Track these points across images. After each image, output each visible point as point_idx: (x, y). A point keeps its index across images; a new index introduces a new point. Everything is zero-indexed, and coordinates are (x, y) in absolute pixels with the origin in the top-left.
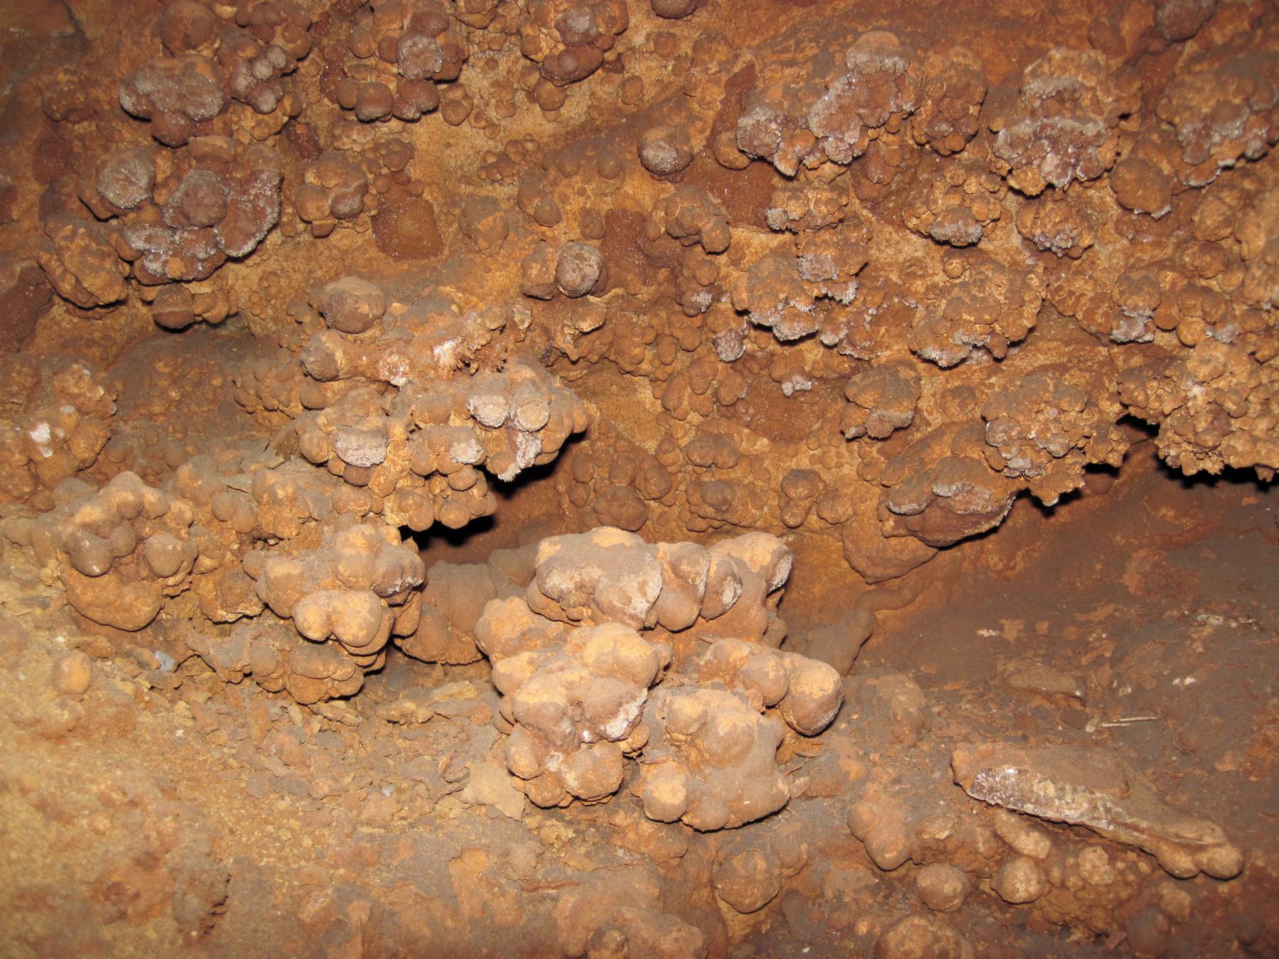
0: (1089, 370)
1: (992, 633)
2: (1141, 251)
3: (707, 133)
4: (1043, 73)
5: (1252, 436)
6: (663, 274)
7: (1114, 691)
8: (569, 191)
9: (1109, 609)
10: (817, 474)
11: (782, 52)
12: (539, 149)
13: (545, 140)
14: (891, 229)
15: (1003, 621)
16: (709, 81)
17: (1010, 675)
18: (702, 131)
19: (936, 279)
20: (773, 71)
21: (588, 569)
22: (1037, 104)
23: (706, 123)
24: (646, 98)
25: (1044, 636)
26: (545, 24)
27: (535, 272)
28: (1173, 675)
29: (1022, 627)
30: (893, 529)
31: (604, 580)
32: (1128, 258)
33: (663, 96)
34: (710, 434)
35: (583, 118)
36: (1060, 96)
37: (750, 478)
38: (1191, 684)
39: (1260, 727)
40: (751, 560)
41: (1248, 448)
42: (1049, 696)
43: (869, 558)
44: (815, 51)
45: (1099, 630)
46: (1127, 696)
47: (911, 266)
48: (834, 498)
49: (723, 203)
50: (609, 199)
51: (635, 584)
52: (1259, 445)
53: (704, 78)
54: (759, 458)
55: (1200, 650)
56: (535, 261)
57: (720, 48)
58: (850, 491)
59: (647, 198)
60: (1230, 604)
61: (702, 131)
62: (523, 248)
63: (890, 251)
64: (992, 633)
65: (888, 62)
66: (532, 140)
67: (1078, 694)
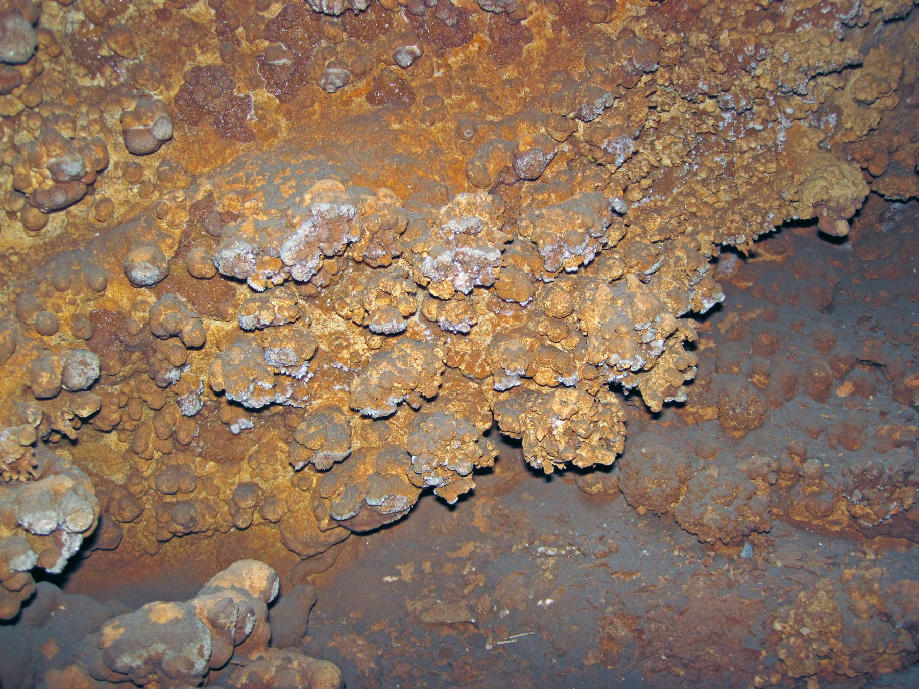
0: (465, 400)
1: (395, 579)
2: (505, 322)
3: (175, 248)
4: (456, 216)
5: (591, 446)
6: (136, 355)
7: (496, 614)
8: (61, 302)
9: (471, 546)
10: (257, 485)
11: (234, 182)
12: (23, 261)
13: (25, 251)
14: (320, 312)
15: (398, 567)
16: (178, 207)
17: (421, 612)
18: (171, 247)
19: (356, 347)
20: (231, 199)
21: (156, 646)
22: (452, 237)
23: (174, 239)
24: (116, 216)
25: (430, 573)
26: (38, 165)
27: (45, 380)
28: (536, 599)
29: (413, 569)
30: (328, 525)
31: (168, 652)
32: (495, 326)
33: (132, 214)
34: (171, 466)
35: (59, 231)
36: (467, 232)
37: (204, 494)
38: (551, 604)
39: (604, 628)
40: (251, 587)
41: (590, 455)
42: (452, 626)
43: (305, 543)
44: (263, 183)
45: (469, 565)
46: (507, 616)
47: (338, 339)
48: (274, 502)
49: (189, 301)
50: (92, 303)
51: (195, 651)
52: (597, 452)
53: (172, 204)
54: (209, 477)
55: (551, 577)
56: (44, 370)
57: (181, 177)
58: (285, 496)
59: (125, 300)
60: (554, 535)
61: (171, 247)
62: (26, 355)
63: (319, 327)
64: (395, 579)
65: (344, 209)
66: (16, 254)
67: (473, 621)
